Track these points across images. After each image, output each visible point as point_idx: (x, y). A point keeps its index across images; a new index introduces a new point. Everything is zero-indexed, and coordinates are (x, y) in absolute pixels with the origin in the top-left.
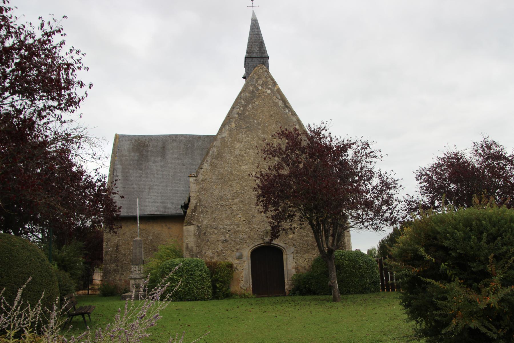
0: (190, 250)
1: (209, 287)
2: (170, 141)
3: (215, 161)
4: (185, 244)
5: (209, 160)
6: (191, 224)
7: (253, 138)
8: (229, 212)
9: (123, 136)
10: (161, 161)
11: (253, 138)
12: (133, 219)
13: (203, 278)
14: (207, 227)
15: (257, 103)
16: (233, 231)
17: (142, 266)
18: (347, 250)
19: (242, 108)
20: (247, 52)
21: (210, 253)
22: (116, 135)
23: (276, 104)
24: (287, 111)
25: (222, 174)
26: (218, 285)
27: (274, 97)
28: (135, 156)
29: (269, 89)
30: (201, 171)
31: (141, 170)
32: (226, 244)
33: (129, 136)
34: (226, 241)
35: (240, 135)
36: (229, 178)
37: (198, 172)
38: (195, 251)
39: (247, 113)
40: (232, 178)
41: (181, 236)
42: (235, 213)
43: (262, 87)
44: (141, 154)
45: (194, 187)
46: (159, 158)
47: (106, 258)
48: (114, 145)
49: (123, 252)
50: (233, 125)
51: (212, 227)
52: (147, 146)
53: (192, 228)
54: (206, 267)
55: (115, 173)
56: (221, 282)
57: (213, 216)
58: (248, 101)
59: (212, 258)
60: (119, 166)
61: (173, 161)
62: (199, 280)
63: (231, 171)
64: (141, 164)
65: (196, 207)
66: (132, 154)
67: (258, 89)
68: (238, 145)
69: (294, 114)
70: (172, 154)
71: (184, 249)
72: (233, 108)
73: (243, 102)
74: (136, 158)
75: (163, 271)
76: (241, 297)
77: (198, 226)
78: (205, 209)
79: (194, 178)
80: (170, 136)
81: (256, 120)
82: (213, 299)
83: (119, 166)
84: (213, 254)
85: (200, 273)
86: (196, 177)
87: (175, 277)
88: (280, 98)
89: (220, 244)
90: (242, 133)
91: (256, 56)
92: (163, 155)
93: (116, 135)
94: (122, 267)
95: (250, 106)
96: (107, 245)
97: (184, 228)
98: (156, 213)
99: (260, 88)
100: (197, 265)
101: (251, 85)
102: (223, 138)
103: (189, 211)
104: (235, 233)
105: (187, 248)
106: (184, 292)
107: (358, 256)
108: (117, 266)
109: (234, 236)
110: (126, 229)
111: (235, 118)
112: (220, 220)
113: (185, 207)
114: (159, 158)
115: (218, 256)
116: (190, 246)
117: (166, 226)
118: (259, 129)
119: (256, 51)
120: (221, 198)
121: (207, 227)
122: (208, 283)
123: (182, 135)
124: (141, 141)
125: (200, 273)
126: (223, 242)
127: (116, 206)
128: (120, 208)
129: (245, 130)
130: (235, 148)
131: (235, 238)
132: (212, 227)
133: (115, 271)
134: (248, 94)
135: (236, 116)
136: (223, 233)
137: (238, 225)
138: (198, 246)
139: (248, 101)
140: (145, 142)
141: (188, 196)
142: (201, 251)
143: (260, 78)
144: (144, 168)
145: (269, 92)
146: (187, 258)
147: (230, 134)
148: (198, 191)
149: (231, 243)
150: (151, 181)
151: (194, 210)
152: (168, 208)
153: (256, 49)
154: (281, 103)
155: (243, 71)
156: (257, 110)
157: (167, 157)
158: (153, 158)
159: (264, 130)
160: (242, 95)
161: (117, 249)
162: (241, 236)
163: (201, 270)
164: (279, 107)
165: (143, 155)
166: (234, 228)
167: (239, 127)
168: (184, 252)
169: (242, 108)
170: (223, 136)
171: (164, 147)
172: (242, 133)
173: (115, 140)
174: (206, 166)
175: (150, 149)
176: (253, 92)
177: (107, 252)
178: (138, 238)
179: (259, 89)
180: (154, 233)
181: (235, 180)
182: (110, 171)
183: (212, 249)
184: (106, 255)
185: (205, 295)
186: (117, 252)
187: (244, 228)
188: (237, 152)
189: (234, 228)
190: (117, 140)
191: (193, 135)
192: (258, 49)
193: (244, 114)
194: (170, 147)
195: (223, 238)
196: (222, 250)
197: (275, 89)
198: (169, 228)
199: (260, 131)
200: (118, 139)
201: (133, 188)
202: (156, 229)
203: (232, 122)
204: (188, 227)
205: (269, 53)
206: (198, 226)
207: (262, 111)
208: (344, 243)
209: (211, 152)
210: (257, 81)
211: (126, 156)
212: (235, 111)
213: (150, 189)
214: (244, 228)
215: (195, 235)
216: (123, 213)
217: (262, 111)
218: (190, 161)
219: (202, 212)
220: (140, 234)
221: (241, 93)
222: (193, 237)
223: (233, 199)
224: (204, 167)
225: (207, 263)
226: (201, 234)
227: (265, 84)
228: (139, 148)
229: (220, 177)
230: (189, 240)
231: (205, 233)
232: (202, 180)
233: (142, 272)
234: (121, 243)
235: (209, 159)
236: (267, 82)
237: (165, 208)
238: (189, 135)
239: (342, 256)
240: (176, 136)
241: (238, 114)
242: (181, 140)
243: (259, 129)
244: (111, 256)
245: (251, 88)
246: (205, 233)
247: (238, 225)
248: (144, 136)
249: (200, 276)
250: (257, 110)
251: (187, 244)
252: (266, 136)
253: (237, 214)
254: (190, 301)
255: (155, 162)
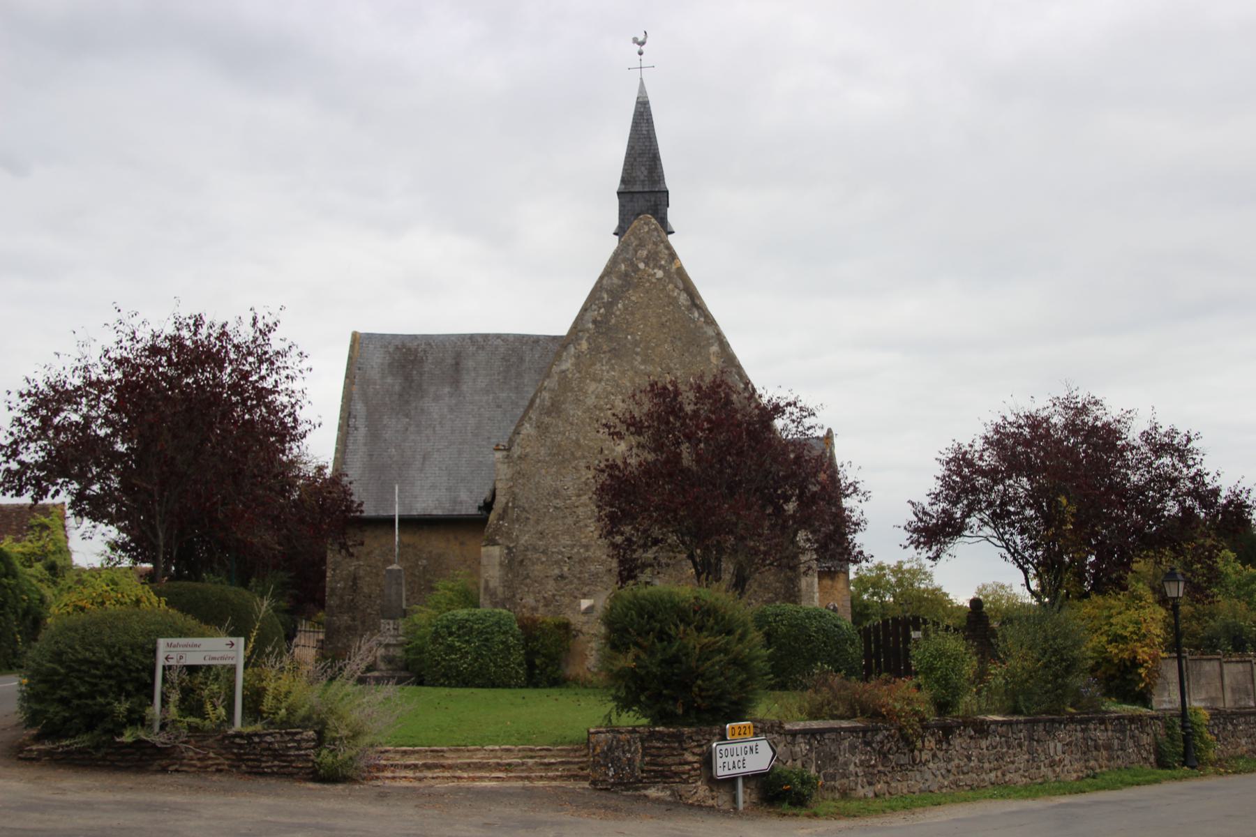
0: (491, 593)
1: (520, 665)
2: (472, 349)
3: (547, 420)
4: (482, 585)
5: (534, 417)
6: (495, 543)
7: (624, 373)
8: (570, 521)
9: (370, 337)
10: (451, 395)
11: (624, 373)
12: (389, 521)
13: (508, 648)
14: (527, 549)
15: (633, 298)
16: (576, 558)
17: (401, 621)
18: (803, 604)
19: (602, 311)
20: (623, 181)
21: (530, 600)
22: (355, 336)
23: (673, 301)
24: (696, 315)
25: (560, 446)
26: (537, 662)
27: (671, 286)
28: (394, 383)
29: (661, 267)
30: (518, 439)
31: (407, 416)
32: (562, 584)
33: (382, 336)
34: (562, 577)
35: (598, 366)
36: (572, 453)
37: (511, 441)
38: (500, 596)
39: (613, 321)
40: (579, 454)
41: (476, 565)
42: (581, 524)
43: (647, 265)
44: (408, 378)
45: (504, 471)
46: (447, 390)
47: (332, 602)
48: (350, 358)
49: (366, 590)
50: (584, 345)
51: (535, 549)
52: (422, 361)
53: (496, 551)
54: (516, 626)
55: (352, 422)
56: (544, 655)
57: (540, 528)
58: (616, 295)
59: (535, 609)
60: (359, 407)
61: (477, 398)
62: (501, 651)
63: (578, 439)
64: (407, 402)
65: (505, 510)
66: (389, 380)
67: (637, 270)
68: (592, 387)
69: (710, 321)
70: (475, 380)
71: (482, 591)
72: (585, 309)
73: (605, 296)
74: (397, 388)
75: (436, 632)
76: (586, 687)
77: (508, 548)
78: (524, 515)
79: (505, 453)
80: (472, 338)
81: (632, 334)
82: (527, 687)
83: (359, 407)
84: (537, 601)
85: (502, 637)
86: (509, 450)
87: (457, 644)
88: (681, 286)
89: (551, 582)
90: (601, 361)
91: (643, 193)
92: (456, 382)
93: (355, 336)
94: (363, 622)
95: (620, 306)
96: (333, 576)
97: (483, 549)
98: (435, 512)
99: (642, 266)
100: (498, 623)
101: (624, 260)
102: (563, 372)
103: (493, 517)
104: (580, 561)
105: (487, 588)
106: (472, 671)
107: (809, 618)
108: (354, 619)
109: (578, 568)
110: (373, 542)
111: (588, 330)
112: (553, 537)
113: (488, 506)
114: (447, 390)
115: (546, 606)
116: (492, 585)
117: (456, 538)
118: (637, 354)
119: (642, 178)
120: (556, 494)
121: (527, 549)
122: (518, 656)
123: (498, 336)
124: (409, 349)
125: (502, 637)
126: (556, 580)
127: (352, 502)
128: (361, 504)
129: (608, 355)
130: (586, 393)
131: (581, 572)
132: (535, 549)
133: (348, 628)
134: (615, 280)
135: (591, 326)
136: (557, 562)
137: (587, 547)
138: (508, 585)
139: (616, 295)
140: (416, 350)
141: (491, 486)
142: (514, 596)
143: (641, 245)
144: (413, 412)
145: (660, 274)
146: (485, 609)
147: (576, 365)
148: (512, 479)
149: (571, 583)
150: (428, 440)
151: (501, 517)
152: (461, 502)
153: (642, 173)
154: (683, 299)
155: (614, 222)
156: (632, 314)
157: (464, 388)
158: (432, 389)
159: (647, 355)
160: (605, 282)
161: (355, 584)
162: (592, 568)
163: (505, 633)
164: (679, 307)
165: (413, 381)
166: (578, 552)
167: (595, 350)
168: (482, 596)
169: (602, 311)
170: (564, 367)
171: (457, 364)
172: (601, 361)
173: (352, 347)
174: (528, 429)
175: (427, 367)
176: (626, 274)
177: (333, 590)
178: (395, 567)
179: (639, 269)
180: (430, 552)
181: (584, 457)
182: (341, 418)
183: (534, 593)
184: (331, 596)
185: (511, 678)
186: (355, 591)
187: (598, 553)
188: (591, 401)
189: (578, 552)
190: (357, 346)
191: (523, 336)
192: (646, 173)
193: (608, 322)
194: (470, 364)
195: (557, 572)
196: (554, 595)
197: (674, 267)
198: (462, 544)
199: (639, 358)
200: (359, 342)
201: (390, 457)
202: (436, 544)
203: (581, 338)
204: (490, 548)
205: (670, 182)
206: (508, 548)
207: (644, 317)
208: (799, 591)
209: (538, 401)
210: (636, 252)
211: (375, 384)
212: (590, 315)
213: (424, 458)
214: (598, 553)
215: (501, 564)
216: (369, 511)
217: (644, 317)
218: (513, 396)
219: (518, 520)
220: (401, 555)
221: (601, 278)
222: (498, 568)
223: (579, 496)
224: (524, 432)
225: (519, 620)
226: (514, 563)
227: (652, 259)
228: (404, 367)
229: (555, 451)
230: (491, 573)
231: (522, 561)
232: (519, 458)
233: (401, 632)
234: (362, 573)
235: (533, 415)
236: (657, 253)
237: (455, 501)
238: (514, 335)
239: (777, 615)
240: (486, 337)
241: (595, 322)
242: (497, 347)
243: (637, 354)
244: (341, 598)
245: (623, 267)
246: (522, 561)
247: (587, 547)
248: (415, 337)
249: (503, 643)
250: (632, 314)
251: (487, 582)
252: (650, 368)
253: (586, 526)
254: (483, 687)
255: (437, 398)
